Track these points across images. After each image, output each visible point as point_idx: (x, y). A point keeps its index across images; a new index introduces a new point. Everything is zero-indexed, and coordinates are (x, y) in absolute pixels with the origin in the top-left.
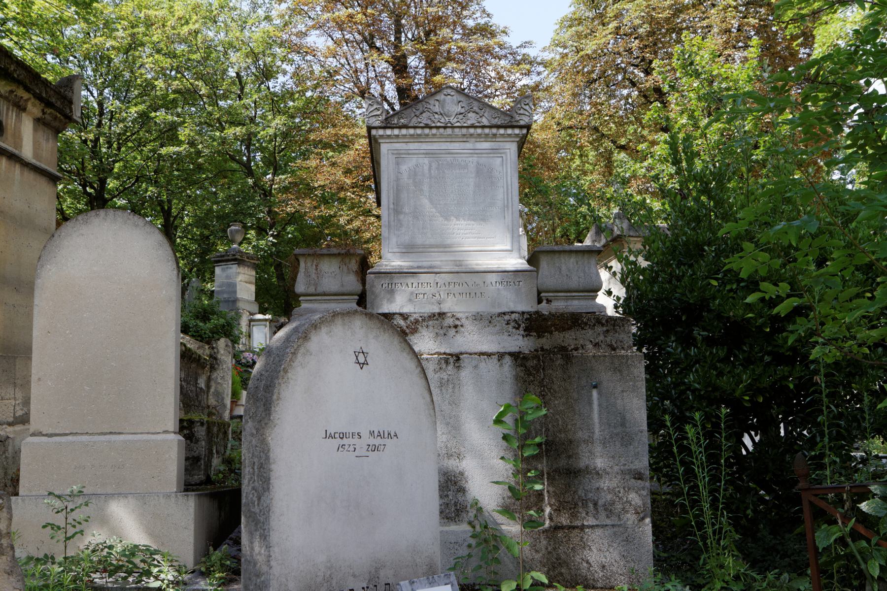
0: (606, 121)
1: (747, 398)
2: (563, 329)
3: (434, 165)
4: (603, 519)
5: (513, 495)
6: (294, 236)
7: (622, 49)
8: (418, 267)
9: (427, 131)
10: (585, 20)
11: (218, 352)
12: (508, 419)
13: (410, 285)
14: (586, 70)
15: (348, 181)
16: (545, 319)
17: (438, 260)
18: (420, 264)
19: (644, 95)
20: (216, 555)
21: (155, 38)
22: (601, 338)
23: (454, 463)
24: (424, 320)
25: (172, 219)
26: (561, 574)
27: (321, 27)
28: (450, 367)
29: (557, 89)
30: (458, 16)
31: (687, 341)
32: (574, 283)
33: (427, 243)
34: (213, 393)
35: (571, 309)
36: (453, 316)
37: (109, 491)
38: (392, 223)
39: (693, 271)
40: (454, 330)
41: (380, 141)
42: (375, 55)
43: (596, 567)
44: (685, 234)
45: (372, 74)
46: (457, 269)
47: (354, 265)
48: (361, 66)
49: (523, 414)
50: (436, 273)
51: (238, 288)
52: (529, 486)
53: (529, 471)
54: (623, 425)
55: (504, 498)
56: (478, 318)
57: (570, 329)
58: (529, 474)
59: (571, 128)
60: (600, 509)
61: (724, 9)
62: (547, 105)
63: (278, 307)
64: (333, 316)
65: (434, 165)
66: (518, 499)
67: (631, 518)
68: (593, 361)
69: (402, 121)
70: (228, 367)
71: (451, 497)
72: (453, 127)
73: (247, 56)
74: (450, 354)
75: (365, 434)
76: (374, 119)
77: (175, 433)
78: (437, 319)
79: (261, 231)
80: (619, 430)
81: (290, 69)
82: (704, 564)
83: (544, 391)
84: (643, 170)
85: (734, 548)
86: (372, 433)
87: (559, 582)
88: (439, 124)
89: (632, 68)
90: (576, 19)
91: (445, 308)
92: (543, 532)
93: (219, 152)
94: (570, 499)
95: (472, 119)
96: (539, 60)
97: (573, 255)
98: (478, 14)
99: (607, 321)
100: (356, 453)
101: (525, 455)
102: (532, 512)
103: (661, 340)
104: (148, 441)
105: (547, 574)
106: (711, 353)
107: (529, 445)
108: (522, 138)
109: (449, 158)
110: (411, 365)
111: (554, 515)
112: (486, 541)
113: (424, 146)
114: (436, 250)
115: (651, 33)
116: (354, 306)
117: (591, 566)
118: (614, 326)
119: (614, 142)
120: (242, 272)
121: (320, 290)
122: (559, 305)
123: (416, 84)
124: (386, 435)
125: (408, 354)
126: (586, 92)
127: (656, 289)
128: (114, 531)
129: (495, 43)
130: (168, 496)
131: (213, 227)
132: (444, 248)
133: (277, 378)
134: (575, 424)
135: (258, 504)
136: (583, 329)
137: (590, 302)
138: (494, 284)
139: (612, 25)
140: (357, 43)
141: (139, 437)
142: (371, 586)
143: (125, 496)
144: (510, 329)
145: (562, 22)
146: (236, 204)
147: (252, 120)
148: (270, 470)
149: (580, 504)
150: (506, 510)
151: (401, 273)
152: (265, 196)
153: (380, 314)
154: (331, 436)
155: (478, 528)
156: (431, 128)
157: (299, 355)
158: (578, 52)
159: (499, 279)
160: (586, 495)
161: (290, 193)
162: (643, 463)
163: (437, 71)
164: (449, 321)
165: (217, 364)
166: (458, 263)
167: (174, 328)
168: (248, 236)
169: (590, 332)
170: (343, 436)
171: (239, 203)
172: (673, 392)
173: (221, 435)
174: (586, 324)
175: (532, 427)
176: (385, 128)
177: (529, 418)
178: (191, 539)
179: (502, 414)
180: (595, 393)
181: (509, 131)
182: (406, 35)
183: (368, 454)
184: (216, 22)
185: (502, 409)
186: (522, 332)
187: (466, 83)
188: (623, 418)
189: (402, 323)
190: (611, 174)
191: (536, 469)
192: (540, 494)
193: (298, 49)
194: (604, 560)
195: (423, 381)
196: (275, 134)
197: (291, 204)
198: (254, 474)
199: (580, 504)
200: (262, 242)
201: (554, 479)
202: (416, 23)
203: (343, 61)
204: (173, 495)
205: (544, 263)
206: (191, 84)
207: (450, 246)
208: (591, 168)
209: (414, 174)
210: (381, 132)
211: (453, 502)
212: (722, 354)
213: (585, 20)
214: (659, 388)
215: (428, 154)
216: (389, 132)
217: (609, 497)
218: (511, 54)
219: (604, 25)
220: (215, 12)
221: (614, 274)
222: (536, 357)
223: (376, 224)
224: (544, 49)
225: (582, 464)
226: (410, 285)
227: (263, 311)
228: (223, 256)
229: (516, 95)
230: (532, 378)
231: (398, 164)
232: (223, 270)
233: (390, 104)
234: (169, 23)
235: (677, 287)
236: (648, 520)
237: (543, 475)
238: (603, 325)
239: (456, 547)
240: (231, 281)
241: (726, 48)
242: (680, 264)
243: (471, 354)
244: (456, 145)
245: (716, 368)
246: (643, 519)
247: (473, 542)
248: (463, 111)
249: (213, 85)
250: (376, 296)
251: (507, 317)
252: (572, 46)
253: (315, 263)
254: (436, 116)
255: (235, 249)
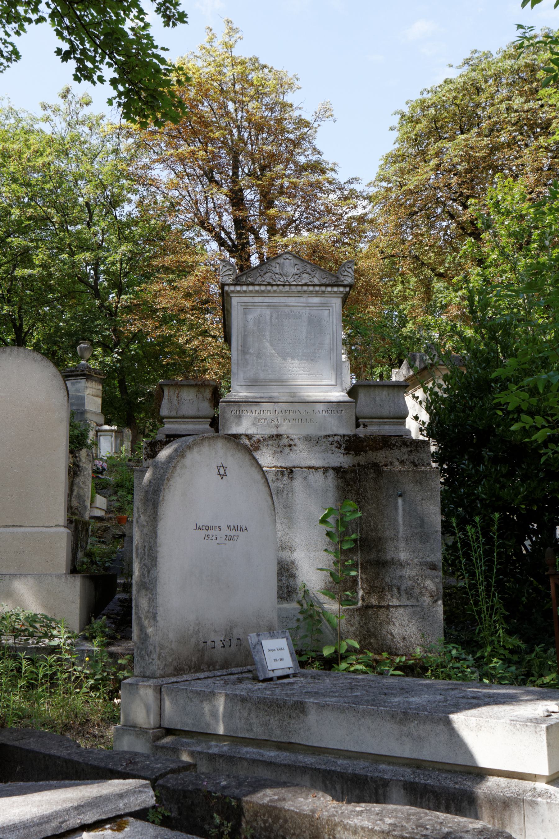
0: (426, 250)
1: (523, 507)
2: (376, 449)
3: (274, 315)
4: (404, 601)
5: (334, 580)
6: (137, 353)
7: (441, 185)
8: (261, 398)
9: (269, 288)
10: (408, 156)
11: (80, 460)
12: (330, 520)
13: (254, 412)
14: (408, 203)
15: (188, 304)
16: (361, 441)
17: (276, 392)
18: (262, 395)
19: (462, 226)
20: (98, 623)
21: (12, 169)
22: (406, 456)
23: (287, 554)
24: (264, 440)
25: (23, 335)
26: (370, 643)
27: (165, 161)
28: (285, 478)
29: (381, 220)
30: (291, 153)
31: (477, 460)
32: (385, 411)
33: (268, 378)
34: (76, 496)
35: (383, 433)
36: (288, 437)
37: (13, 572)
38: (240, 362)
39: (482, 402)
40: (289, 448)
41: (231, 295)
42: (215, 190)
43: (398, 639)
44: (477, 372)
45: (211, 205)
46: (291, 400)
47: (208, 394)
48: (200, 197)
49: (342, 516)
50: (275, 403)
51: (86, 400)
52: (346, 573)
53: (347, 561)
54: (422, 526)
55: (326, 583)
56: (308, 439)
57: (381, 449)
58: (346, 563)
59: (393, 256)
60: (403, 593)
61: (535, 149)
62: (372, 234)
63: (121, 418)
64: (202, 440)
65: (274, 315)
66: (337, 583)
67: (427, 600)
68: (399, 474)
69: (250, 279)
70: (89, 474)
71: (284, 581)
72: (290, 285)
73: (97, 188)
74: (285, 468)
75: (224, 527)
76: (227, 278)
77: (64, 527)
78: (275, 440)
79: (107, 349)
80: (418, 530)
81: (135, 198)
82: (479, 633)
83: (359, 498)
84: (458, 299)
85: (503, 622)
86: (229, 527)
87: (368, 650)
88: (279, 283)
89: (451, 202)
90: (400, 156)
91: (283, 430)
92: (357, 610)
93: (69, 275)
94: (379, 584)
95: (306, 278)
96: (365, 194)
97: (386, 389)
98: (309, 152)
99: (411, 443)
100: (218, 541)
101: (344, 548)
102: (348, 593)
103: (456, 458)
104: (43, 533)
105: (359, 643)
106: (496, 470)
107: (347, 541)
108: (345, 295)
109: (287, 310)
110: (258, 476)
111: (366, 597)
112: (311, 616)
113: (267, 300)
114: (275, 384)
115: (469, 171)
116: (208, 426)
117: (394, 637)
118: (416, 447)
119: (433, 270)
120: (90, 386)
121: (180, 413)
122: (374, 429)
123: (252, 216)
124: (239, 529)
125: (256, 468)
126: (408, 223)
127: (452, 417)
128: (18, 602)
129: (325, 179)
130: (59, 576)
131: (63, 343)
132: (281, 382)
133: (163, 485)
134: (384, 525)
135: (148, 576)
136: (391, 449)
137: (402, 427)
138: (321, 412)
139: (433, 162)
140: (198, 177)
141: (36, 529)
142: (227, 640)
143: (25, 576)
144: (334, 448)
145: (387, 157)
146: (83, 323)
147: (100, 247)
148: (157, 552)
149: (387, 588)
150: (328, 592)
151: (247, 402)
152: (111, 315)
153: (229, 435)
154: (199, 528)
155: (305, 606)
156: (272, 285)
157: (178, 468)
158: (401, 187)
159: (325, 409)
160: (391, 581)
161: (134, 313)
162: (437, 557)
163: (270, 205)
164: (285, 441)
165: (79, 471)
166: (293, 395)
167: (65, 443)
168: (96, 353)
169: (398, 452)
170: (208, 528)
171: (87, 321)
172: (465, 501)
173: (84, 532)
174: (394, 445)
175: (350, 527)
176: (235, 285)
177: (348, 519)
178: (78, 611)
179: (326, 516)
180: (400, 500)
181: (335, 289)
182: (243, 170)
183: (226, 542)
184: (67, 155)
185: (326, 512)
186: (343, 451)
187: (297, 214)
188: (422, 521)
189: (247, 442)
190: (429, 300)
191: (352, 560)
192: (354, 580)
193: (142, 180)
194: (405, 633)
195: (267, 489)
196: (121, 260)
197: (135, 324)
198: (144, 554)
199: (387, 588)
200: (108, 359)
201: (366, 568)
202: (252, 159)
203: (184, 193)
204: (64, 576)
205: (362, 395)
206: (44, 211)
207: (287, 381)
208: (412, 293)
209: (258, 322)
210: (232, 288)
211: (285, 585)
212: (504, 470)
213: (408, 156)
214: (455, 497)
215: (269, 306)
216: (238, 288)
217: (410, 583)
218: (340, 189)
219: (425, 161)
220: (67, 146)
221: (421, 403)
222: (354, 471)
223: (213, 344)
224: (369, 185)
225: (388, 557)
226: (254, 412)
227: (108, 422)
228: (73, 371)
229: (343, 227)
230: (350, 488)
231: (245, 314)
232: (73, 384)
233: (228, 234)
234: (25, 156)
235: (469, 415)
236: (440, 602)
237: (357, 565)
238: (407, 446)
239: (288, 620)
240: (79, 394)
241: (537, 186)
242: (472, 396)
243: (301, 468)
244: (293, 299)
245: (499, 482)
246: (436, 601)
247: (301, 617)
248: (298, 272)
249: (62, 210)
250: (227, 421)
251: (331, 439)
252: (396, 181)
253: (176, 392)
254: (277, 276)
255: (83, 365)
